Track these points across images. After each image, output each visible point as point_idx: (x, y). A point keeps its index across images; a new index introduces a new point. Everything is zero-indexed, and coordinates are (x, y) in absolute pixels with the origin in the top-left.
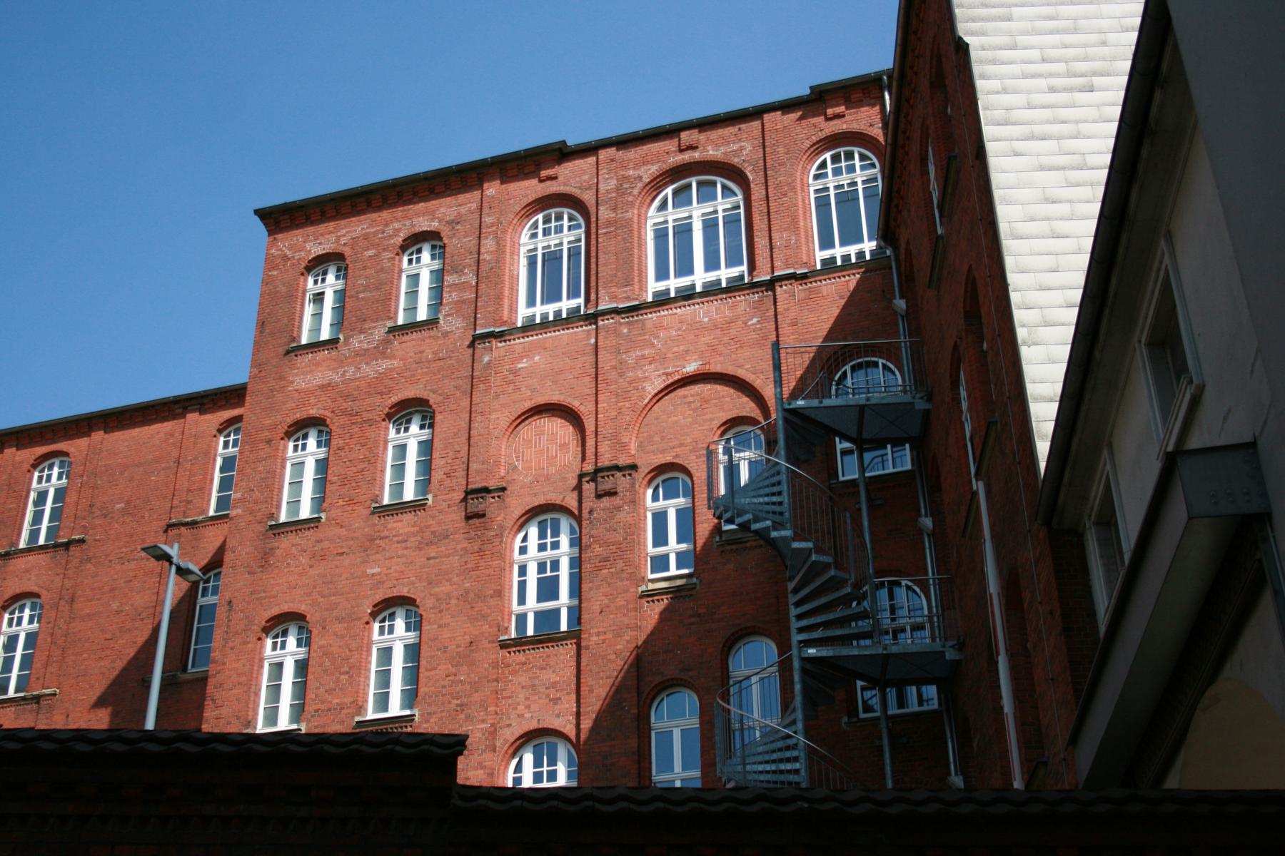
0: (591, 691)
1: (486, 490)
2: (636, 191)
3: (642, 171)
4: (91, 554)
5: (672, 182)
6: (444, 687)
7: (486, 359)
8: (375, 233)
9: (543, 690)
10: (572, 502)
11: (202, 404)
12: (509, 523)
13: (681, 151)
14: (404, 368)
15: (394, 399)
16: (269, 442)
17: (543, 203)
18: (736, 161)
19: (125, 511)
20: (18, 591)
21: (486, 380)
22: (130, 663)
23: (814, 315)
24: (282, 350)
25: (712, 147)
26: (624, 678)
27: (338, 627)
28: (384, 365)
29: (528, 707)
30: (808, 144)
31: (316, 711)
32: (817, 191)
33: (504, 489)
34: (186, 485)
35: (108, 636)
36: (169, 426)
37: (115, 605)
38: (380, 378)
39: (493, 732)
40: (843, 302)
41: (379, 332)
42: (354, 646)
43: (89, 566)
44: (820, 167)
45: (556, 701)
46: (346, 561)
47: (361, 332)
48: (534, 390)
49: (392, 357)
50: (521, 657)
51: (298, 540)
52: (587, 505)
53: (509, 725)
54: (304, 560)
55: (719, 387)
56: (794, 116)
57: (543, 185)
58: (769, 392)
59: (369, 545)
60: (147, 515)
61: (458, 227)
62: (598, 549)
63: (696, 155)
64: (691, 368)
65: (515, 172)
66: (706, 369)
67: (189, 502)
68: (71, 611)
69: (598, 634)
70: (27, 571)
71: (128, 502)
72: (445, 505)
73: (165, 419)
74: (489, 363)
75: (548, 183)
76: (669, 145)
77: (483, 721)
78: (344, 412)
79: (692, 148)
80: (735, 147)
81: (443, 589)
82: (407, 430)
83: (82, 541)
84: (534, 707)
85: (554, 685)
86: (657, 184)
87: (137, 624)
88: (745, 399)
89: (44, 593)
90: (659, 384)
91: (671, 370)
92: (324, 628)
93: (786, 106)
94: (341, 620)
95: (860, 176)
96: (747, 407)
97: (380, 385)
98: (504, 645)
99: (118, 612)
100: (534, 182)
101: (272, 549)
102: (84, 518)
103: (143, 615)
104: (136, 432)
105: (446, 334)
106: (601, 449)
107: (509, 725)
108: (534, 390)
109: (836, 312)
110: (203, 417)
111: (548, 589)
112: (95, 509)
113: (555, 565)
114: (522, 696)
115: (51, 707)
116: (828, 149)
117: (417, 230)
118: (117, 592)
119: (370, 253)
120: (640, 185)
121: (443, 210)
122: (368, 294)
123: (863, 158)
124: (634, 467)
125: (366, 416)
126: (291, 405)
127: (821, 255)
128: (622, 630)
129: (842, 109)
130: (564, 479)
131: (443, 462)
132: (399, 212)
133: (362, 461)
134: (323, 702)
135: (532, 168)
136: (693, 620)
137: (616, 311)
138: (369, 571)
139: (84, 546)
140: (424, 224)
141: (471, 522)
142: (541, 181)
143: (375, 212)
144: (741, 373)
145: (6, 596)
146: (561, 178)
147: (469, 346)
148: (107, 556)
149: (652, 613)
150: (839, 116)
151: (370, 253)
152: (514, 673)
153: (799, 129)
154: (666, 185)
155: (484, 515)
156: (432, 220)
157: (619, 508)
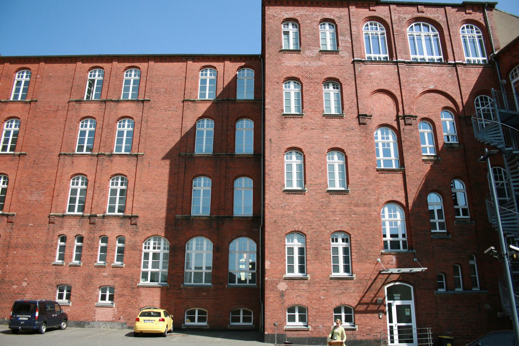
0: (411, 190)
1: (366, 115)
2: (404, 22)
3: (406, 16)
4: (153, 106)
5: (415, 22)
6: (358, 182)
7: (359, 69)
8: (309, 15)
9: (392, 187)
10: (395, 125)
11: (194, 59)
12: (374, 128)
13: (418, 12)
14: (333, 66)
15: (326, 77)
16: (278, 83)
17: (417, 20)
18: (437, 20)
19: (165, 92)
20: (124, 115)
21: (360, 77)
22: (173, 148)
23: (471, 78)
24: (278, 51)
25: (430, 13)
26: (421, 188)
27: (315, 155)
28: (320, 63)
29: (388, 192)
30: (460, 20)
31: (311, 184)
32: (365, 34)
33: (371, 116)
34: (190, 87)
35: (163, 137)
36: (180, 64)
37: (165, 126)
38: (319, 67)
39: (377, 200)
40: (478, 76)
41: (316, 51)
42: (322, 163)
43: (152, 110)
44: (462, 29)
45: (397, 192)
46: (315, 132)
47: (309, 49)
48: (378, 84)
49: (323, 61)
50: (383, 175)
51: (295, 121)
52: (402, 127)
53: (382, 198)
54: (299, 129)
55: (439, 95)
56: (455, 10)
57: (371, 12)
58: (458, 100)
59: (323, 127)
60: (174, 95)
61: (341, 20)
62: (408, 143)
63: (424, 15)
64: (432, 87)
65: (360, 5)
66: (435, 88)
67: (191, 93)
68: (147, 125)
69: (411, 171)
70: (127, 108)
71: (166, 89)
72: (350, 118)
73: (178, 62)
74: (361, 71)
75: (468, 15)
76: (414, 9)
77: (374, 196)
78: (306, 77)
79: (422, 12)
80: (437, 15)
81: (354, 147)
82: (328, 88)
83: (149, 101)
84: (390, 193)
85: (396, 186)
86: (410, 21)
87: (174, 134)
88: (449, 101)
89: (134, 117)
90: (421, 91)
91: (425, 86)
92: (310, 155)
93: (453, 6)
94: (316, 153)
95: (379, 32)
96: (450, 104)
97: (320, 70)
98: (378, 170)
99: (166, 129)
100: (367, 10)
101: (285, 123)
102: (149, 92)
103: (177, 131)
104: (167, 64)
105: (342, 57)
106: (405, 108)
107: (382, 198)
108: (378, 84)
109: (476, 79)
110: (194, 63)
111: (387, 153)
112: (152, 90)
113: (388, 145)
114: (385, 188)
115: (143, 160)
116: (465, 23)
117: (325, 17)
118: (165, 121)
119: (308, 21)
120: (406, 20)
121: (334, 12)
122: (309, 36)
123: (476, 29)
124: (416, 117)
125: (316, 80)
126: (284, 71)
127: (367, 55)
128: (418, 172)
129: (471, 11)
130: (391, 117)
131: (348, 103)
132: (318, 9)
133: (317, 96)
134: (313, 181)
135: (366, 5)
136: (440, 171)
137: (404, 62)
138: (325, 137)
139: (150, 103)
140: (327, 16)
141: (361, 126)
142: (370, 10)
143: (319, 7)
144: (448, 92)
145: (119, 116)
146: (377, 11)
147: (352, 63)
148: (159, 108)
149: (427, 167)
150: (470, 14)
151: (308, 21)
152: (382, 180)
153: (457, 15)
154: (413, 22)
155: (366, 124)
156: (331, 15)
157: (413, 130)
